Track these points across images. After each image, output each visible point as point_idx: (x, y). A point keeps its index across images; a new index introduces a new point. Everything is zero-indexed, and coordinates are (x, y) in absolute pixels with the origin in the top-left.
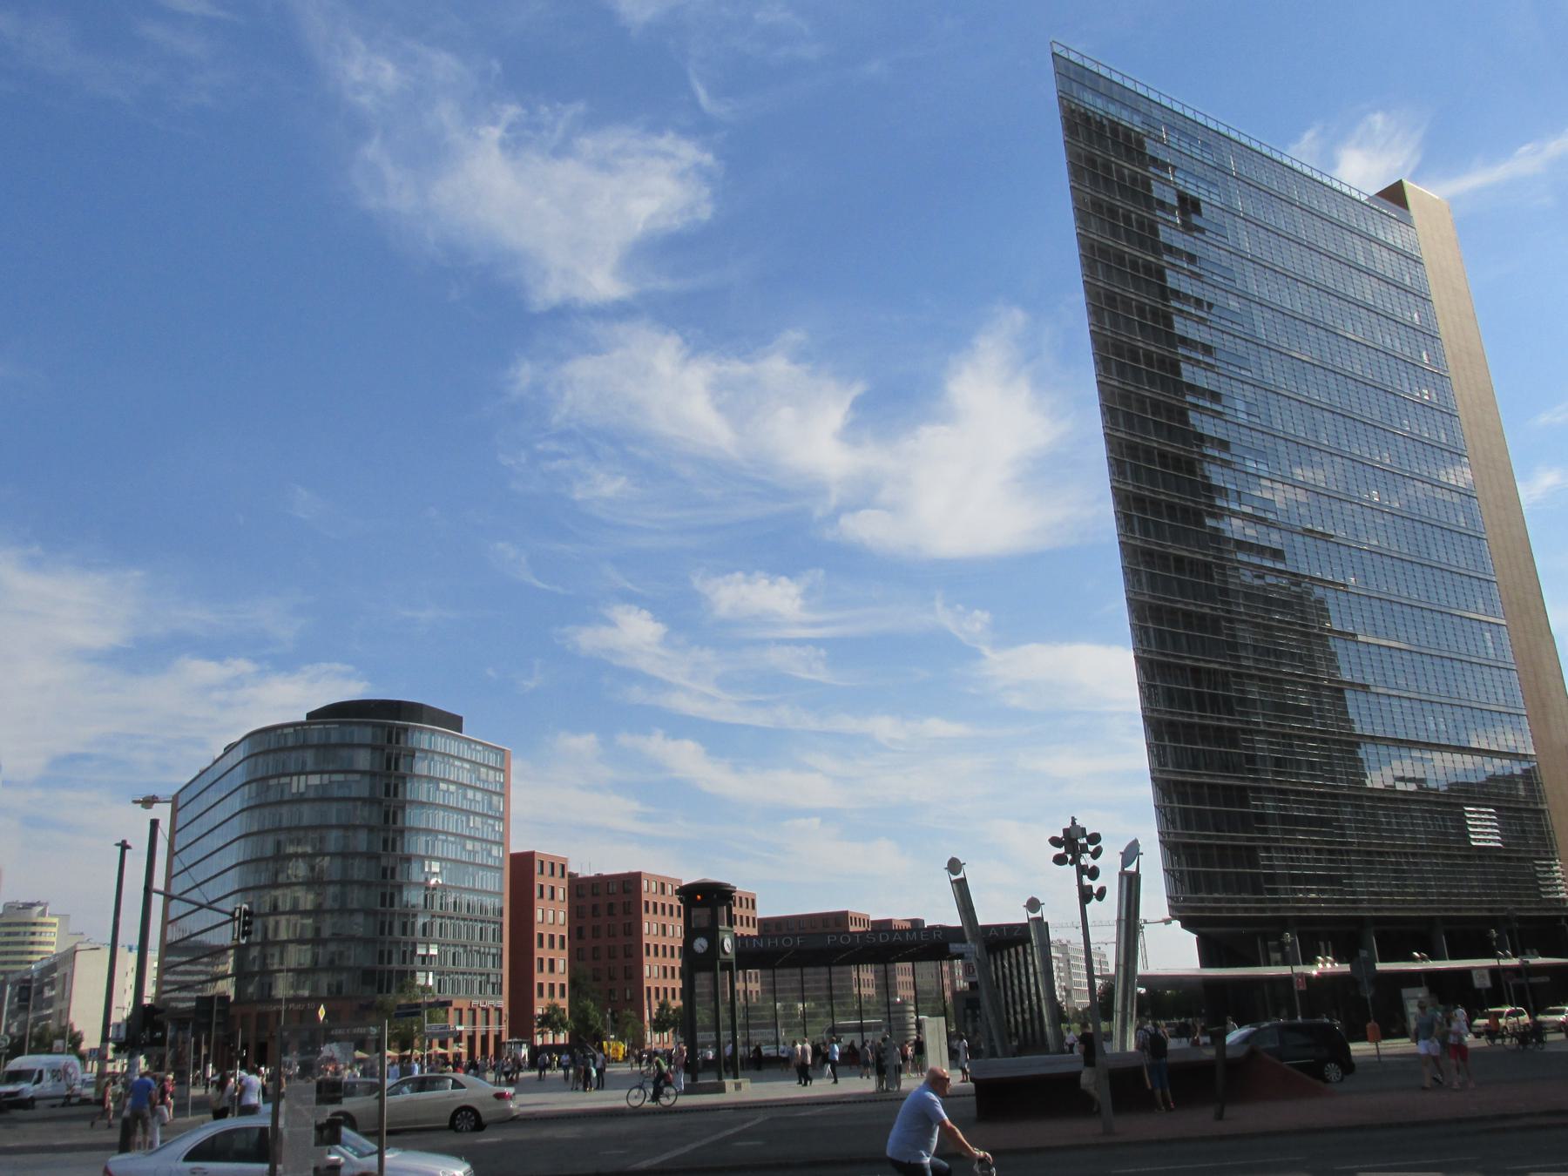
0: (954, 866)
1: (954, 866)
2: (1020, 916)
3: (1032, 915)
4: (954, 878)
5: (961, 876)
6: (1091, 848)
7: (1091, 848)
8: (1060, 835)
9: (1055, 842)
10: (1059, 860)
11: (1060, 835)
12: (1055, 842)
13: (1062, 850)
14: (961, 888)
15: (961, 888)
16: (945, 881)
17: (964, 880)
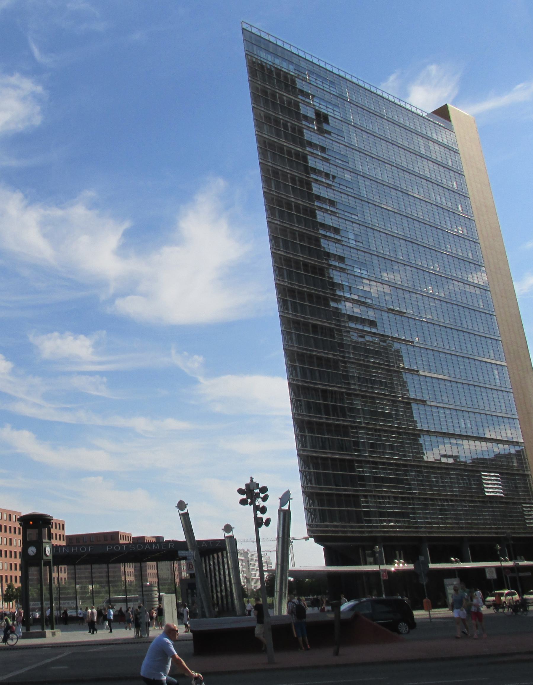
0: (181, 505)
1: (181, 505)
2: (220, 535)
3: (227, 535)
4: (181, 512)
5: (185, 511)
6: (262, 495)
7: (262, 495)
8: (244, 487)
9: (241, 491)
10: (243, 502)
11: (244, 487)
12: (241, 491)
13: (245, 497)
14: (186, 519)
15: (186, 519)
16: (176, 514)
17: (187, 514)
